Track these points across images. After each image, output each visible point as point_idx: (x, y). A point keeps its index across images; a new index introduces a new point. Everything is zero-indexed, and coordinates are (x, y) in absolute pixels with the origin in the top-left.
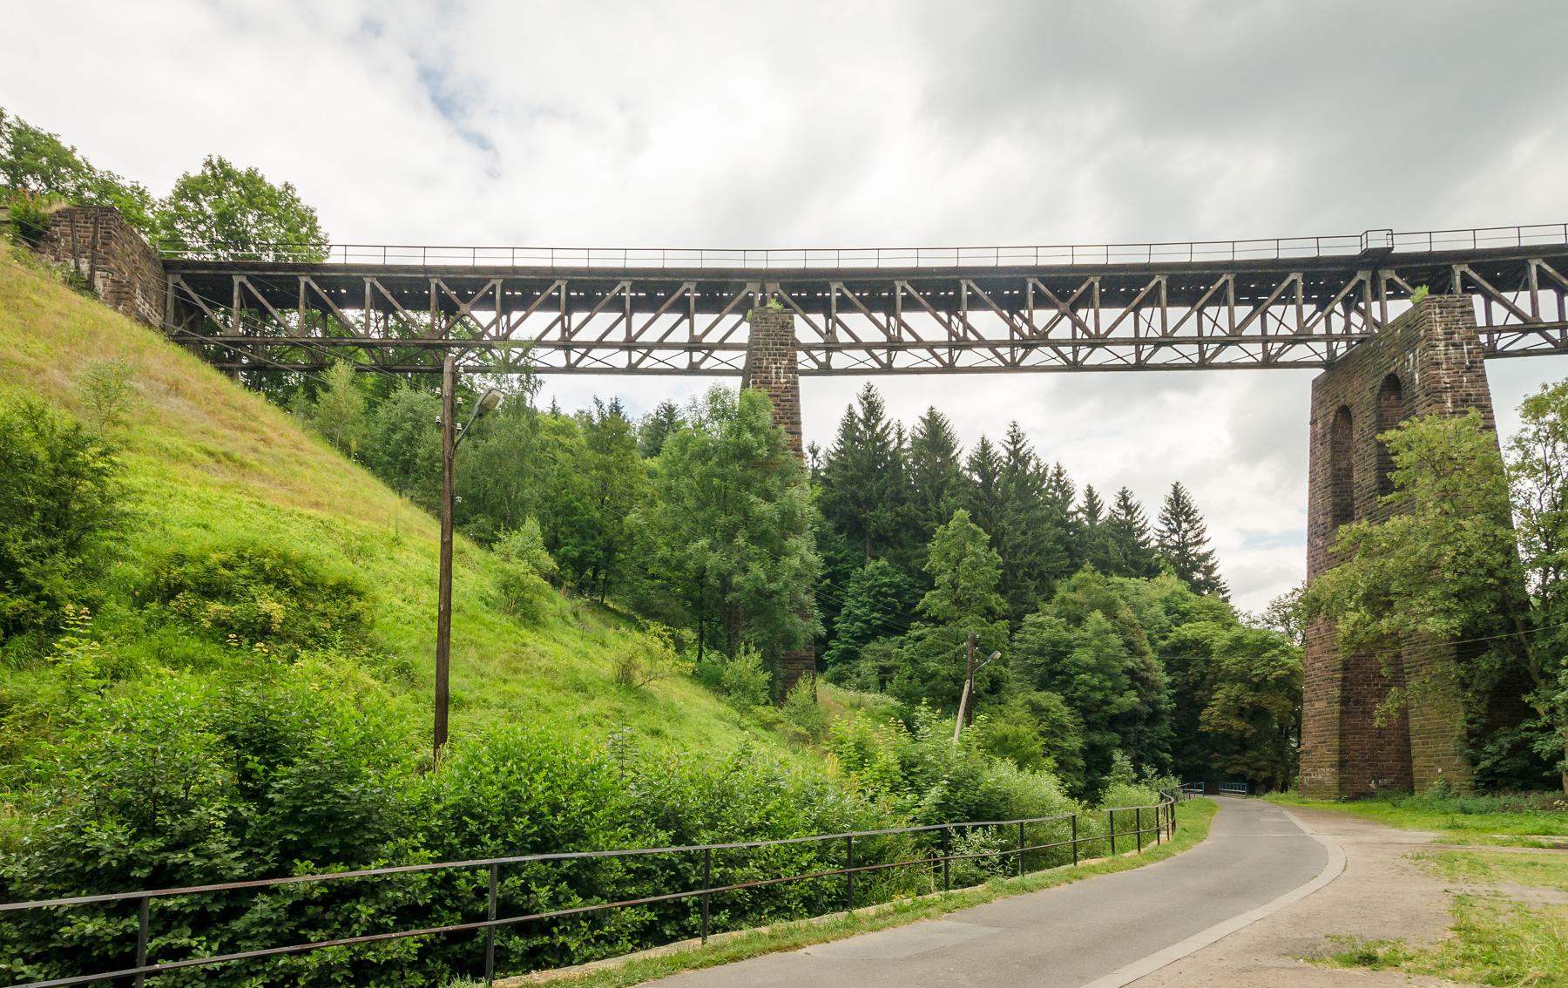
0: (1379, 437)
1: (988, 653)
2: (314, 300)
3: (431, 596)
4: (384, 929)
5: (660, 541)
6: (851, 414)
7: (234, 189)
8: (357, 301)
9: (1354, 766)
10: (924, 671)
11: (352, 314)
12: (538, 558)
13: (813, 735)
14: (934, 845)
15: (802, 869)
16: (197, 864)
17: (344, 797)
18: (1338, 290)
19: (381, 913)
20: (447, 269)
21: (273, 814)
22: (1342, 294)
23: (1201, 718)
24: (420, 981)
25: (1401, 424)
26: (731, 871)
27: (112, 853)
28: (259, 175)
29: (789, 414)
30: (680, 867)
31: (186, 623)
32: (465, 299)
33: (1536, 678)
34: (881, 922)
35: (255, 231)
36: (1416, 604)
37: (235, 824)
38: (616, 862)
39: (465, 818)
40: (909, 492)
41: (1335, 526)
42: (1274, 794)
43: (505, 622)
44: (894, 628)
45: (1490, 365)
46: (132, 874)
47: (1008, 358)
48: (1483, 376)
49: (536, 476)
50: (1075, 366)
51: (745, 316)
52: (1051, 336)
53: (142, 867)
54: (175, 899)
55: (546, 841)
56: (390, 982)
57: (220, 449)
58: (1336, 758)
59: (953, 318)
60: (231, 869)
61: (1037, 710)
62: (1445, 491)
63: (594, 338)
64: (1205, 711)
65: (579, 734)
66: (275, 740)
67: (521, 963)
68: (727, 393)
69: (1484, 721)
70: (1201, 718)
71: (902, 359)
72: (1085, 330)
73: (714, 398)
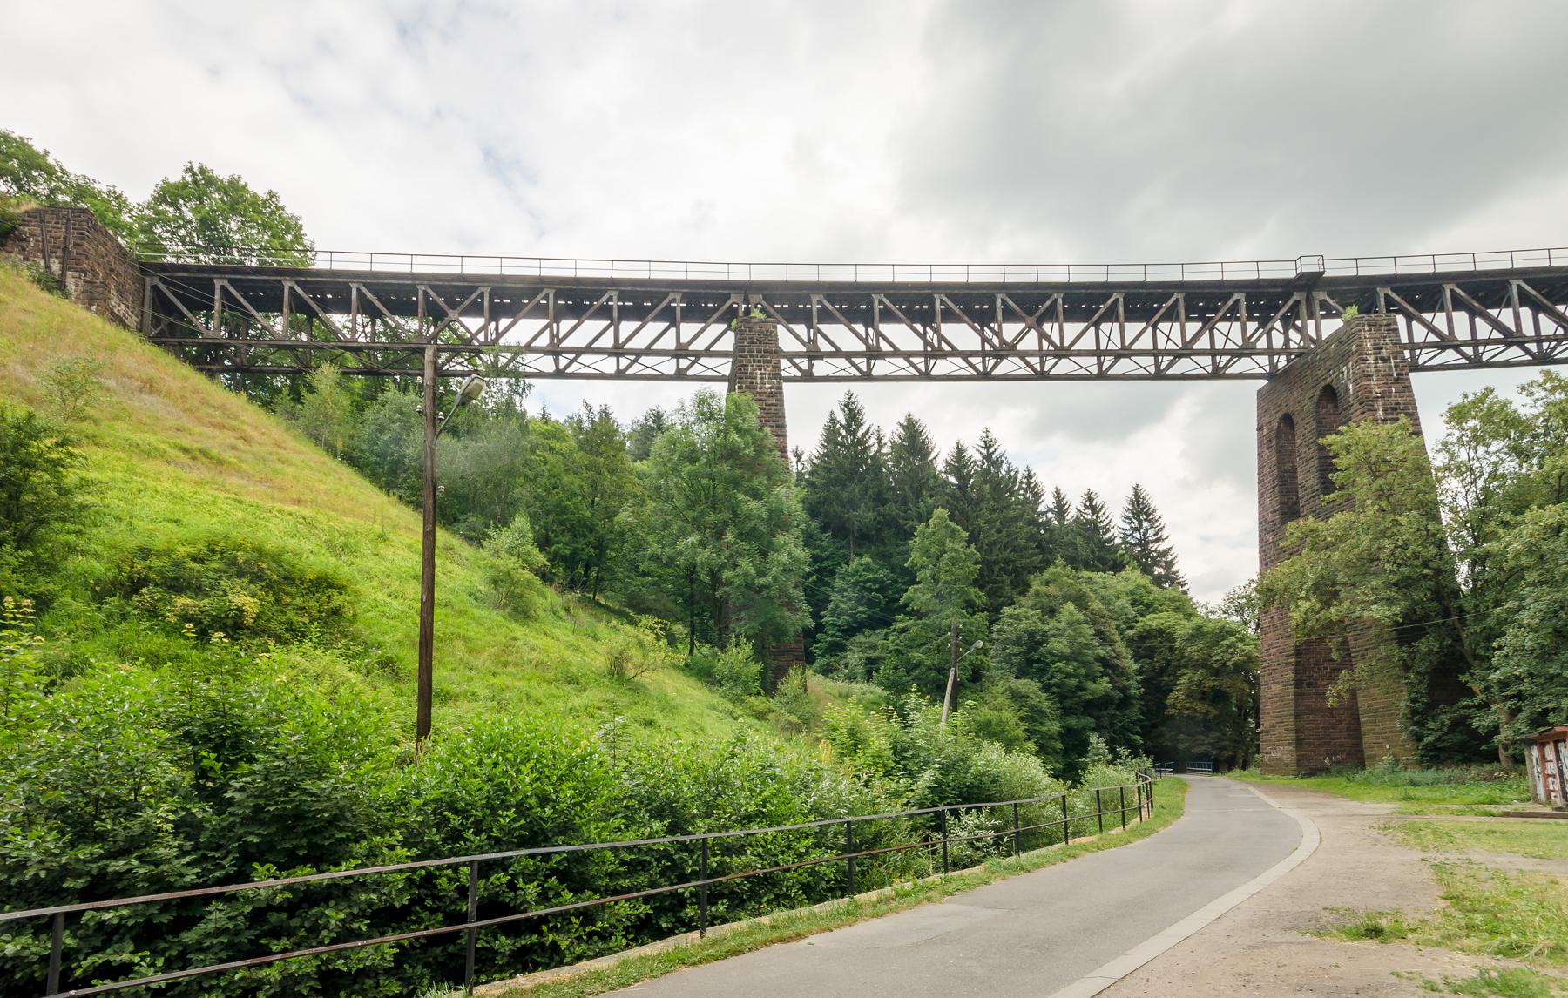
0: (1321, 441)
1: (969, 643)
2: (299, 305)
3: (414, 590)
4: (358, 935)
5: (650, 539)
6: (833, 420)
7: (216, 196)
8: (343, 306)
9: (1310, 744)
10: (908, 662)
11: (339, 320)
12: (528, 553)
13: (804, 723)
14: (928, 828)
15: (800, 856)
16: (142, 871)
17: (312, 794)
18: (1277, 309)
19: (354, 917)
20: (435, 277)
21: (232, 814)
22: (1281, 313)
23: (1168, 702)
24: (396, 989)
25: (1340, 428)
26: (728, 860)
27: (41, 862)
28: (242, 183)
29: (774, 415)
30: (676, 857)
31: (150, 618)
32: (454, 306)
33: (1470, 660)
34: (883, 907)
35: (237, 236)
36: (1361, 592)
37: (187, 827)
38: (609, 854)
39: (446, 813)
40: (890, 493)
41: (1284, 522)
42: (1237, 772)
43: (496, 617)
44: (880, 621)
45: (1415, 378)
46: (65, 885)
47: (980, 367)
48: (1408, 388)
49: (526, 477)
50: (1042, 376)
51: (729, 326)
52: (1020, 347)
53: (77, 875)
54: (113, 911)
55: (534, 834)
56: (362, 992)
57: (196, 446)
58: (1292, 736)
59: (928, 329)
60: (182, 876)
61: (1016, 696)
62: (1382, 490)
63: (583, 345)
64: (1171, 696)
65: (571, 724)
66: (237, 735)
67: (508, 964)
68: (713, 396)
69: (1425, 700)
70: (1168, 702)
71: (880, 367)
72: (1051, 342)
73: (701, 401)
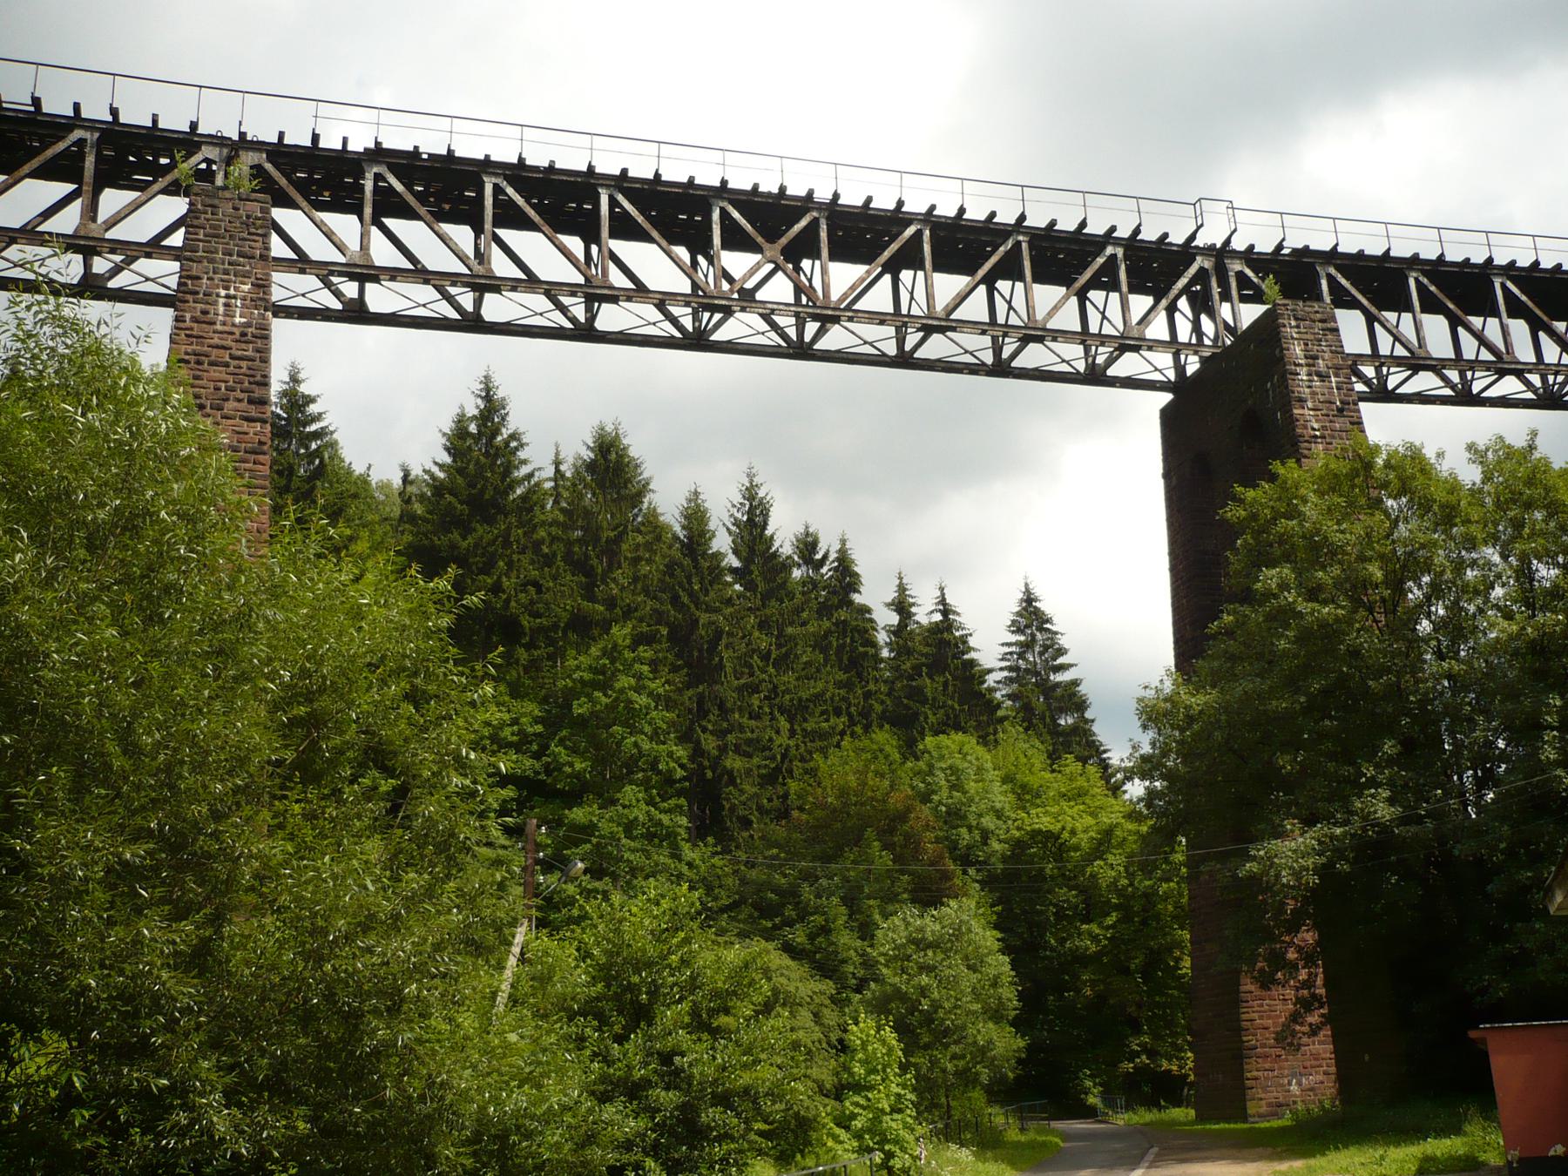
48: (1359, 423)
